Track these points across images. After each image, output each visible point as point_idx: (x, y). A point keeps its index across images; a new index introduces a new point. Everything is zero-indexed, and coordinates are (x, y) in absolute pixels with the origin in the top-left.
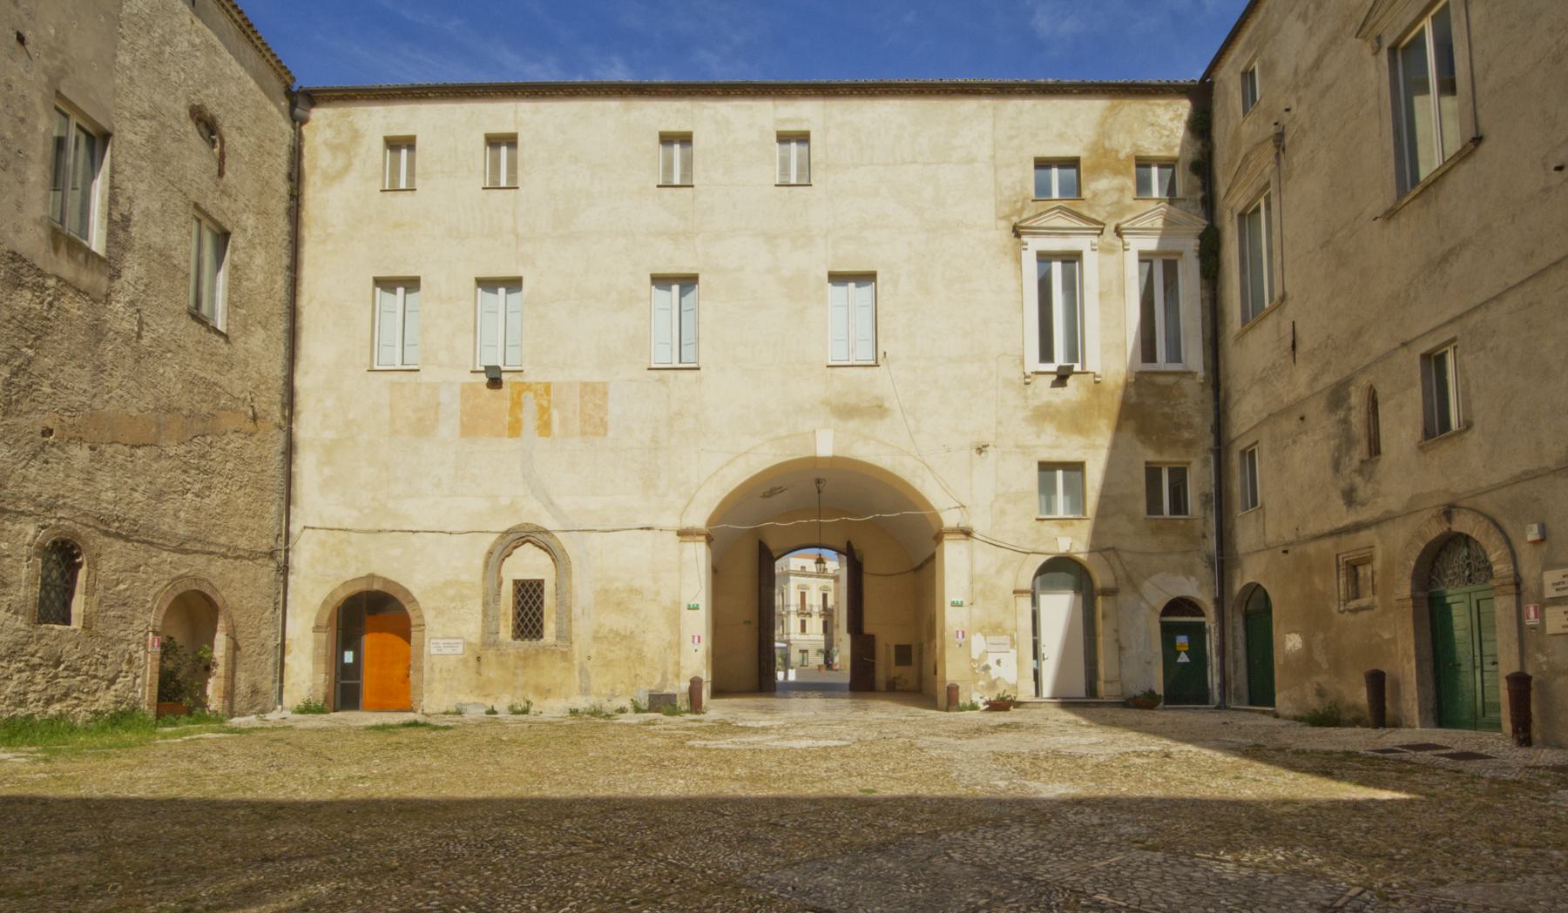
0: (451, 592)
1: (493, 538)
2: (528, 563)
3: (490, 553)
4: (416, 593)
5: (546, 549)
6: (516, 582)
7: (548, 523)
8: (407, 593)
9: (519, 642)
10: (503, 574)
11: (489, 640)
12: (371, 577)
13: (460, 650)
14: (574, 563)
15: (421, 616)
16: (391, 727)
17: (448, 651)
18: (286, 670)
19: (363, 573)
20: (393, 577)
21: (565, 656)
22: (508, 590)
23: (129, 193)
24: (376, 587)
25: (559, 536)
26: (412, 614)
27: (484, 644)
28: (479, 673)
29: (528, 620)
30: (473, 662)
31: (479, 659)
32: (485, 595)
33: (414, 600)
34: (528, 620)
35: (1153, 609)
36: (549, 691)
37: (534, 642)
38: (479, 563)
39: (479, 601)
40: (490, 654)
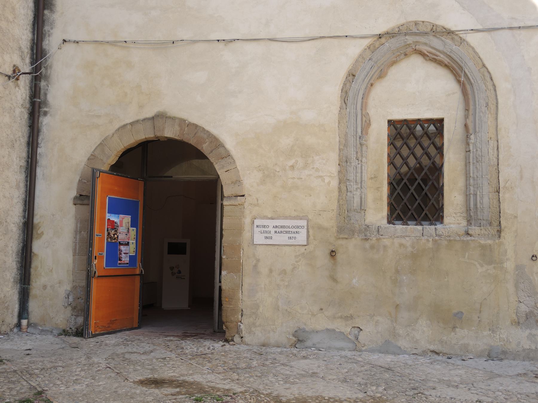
0: (286, 142)
1: (355, 49)
2: (418, 92)
3: (352, 75)
4: (230, 143)
5: (454, 68)
6: (391, 123)
7: (455, 19)
8: (217, 143)
9: (399, 227)
10: (372, 111)
11: (348, 223)
12: (160, 117)
13: (301, 238)
14: (503, 86)
15: (238, 182)
16: (467, 186)
17: (282, 239)
18: (35, 263)
19: (149, 113)
20: (194, 118)
21: (488, 256)
22: (379, 137)
23: (450, 50)
24: (170, 132)
25: (472, 39)
26: (224, 177)
27: (340, 230)
28: (334, 279)
29: (416, 191)
30: (322, 258)
31: (333, 254)
32: (344, 145)
33: (228, 155)
34: (416, 191)
35: (51, 115)
36: (459, 316)
37: (429, 229)
38: (332, 92)
39: (334, 157)
40: (351, 247)
